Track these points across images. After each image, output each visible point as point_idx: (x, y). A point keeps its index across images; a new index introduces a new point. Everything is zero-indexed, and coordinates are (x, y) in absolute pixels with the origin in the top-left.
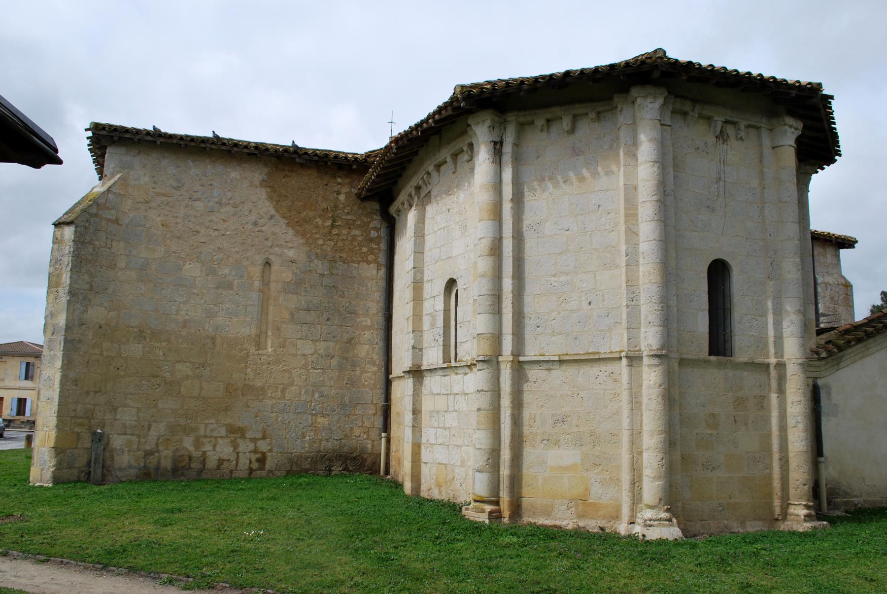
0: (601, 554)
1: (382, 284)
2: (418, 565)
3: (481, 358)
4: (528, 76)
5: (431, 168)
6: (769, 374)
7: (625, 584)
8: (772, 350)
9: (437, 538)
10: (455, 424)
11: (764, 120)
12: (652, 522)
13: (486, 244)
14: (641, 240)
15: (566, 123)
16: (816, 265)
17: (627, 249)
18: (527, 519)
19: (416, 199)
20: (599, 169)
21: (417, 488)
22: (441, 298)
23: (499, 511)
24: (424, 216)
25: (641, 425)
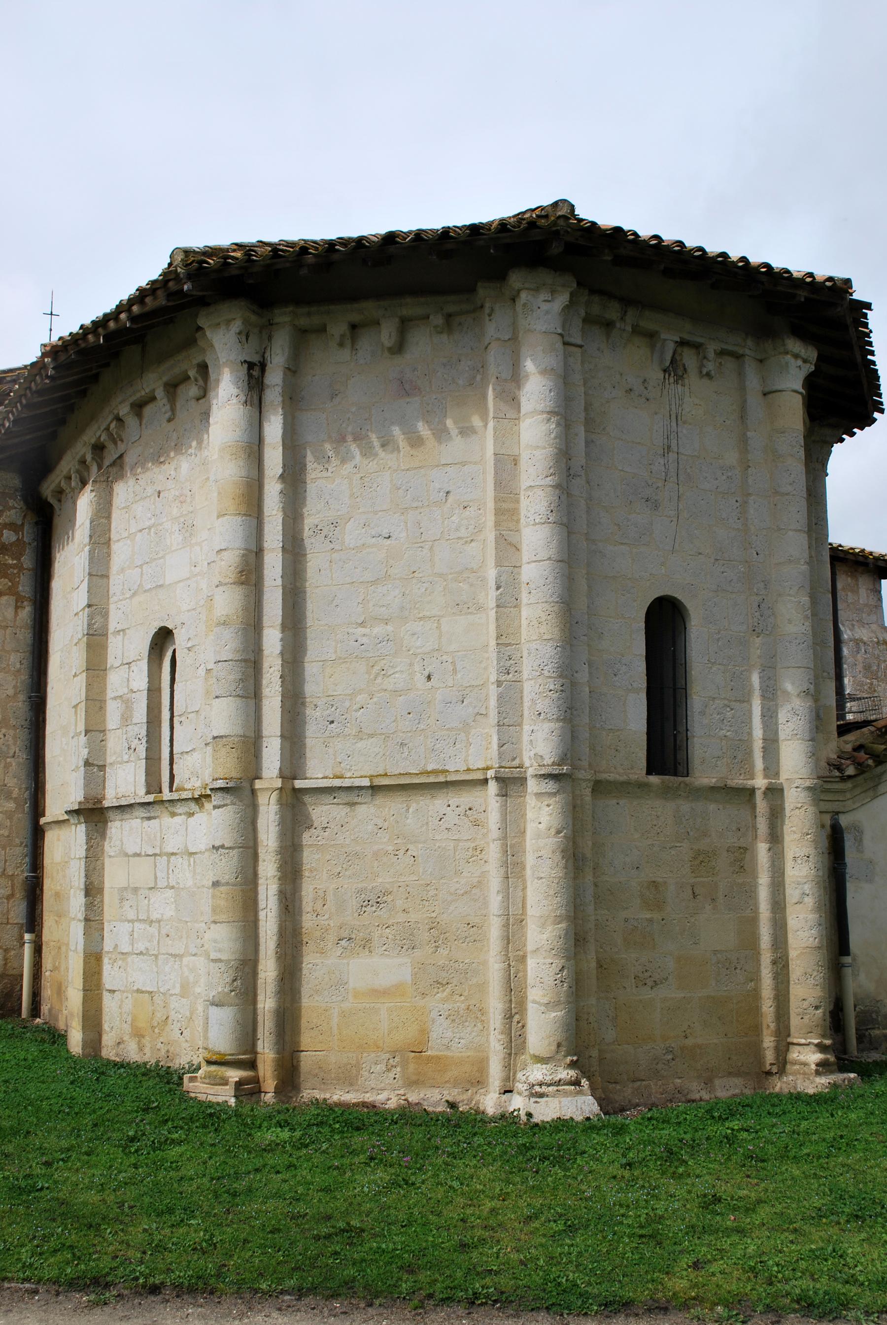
0: (450, 1154)
1: (26, 636)
2: (93, 1197)
3: (220, 784)
4: (317, 238)
5: (124, 410)
6: (754, 807)
7: (493, 1210)
8: (759, 764)
9: (132, 1140)
10: (169, 912)
11: (749, 342)
12: (544, 1089)
13: (230, 561)
14: (525, 559)
15: (387, 334)
16: (840, 606)
17: (499, 576)
18: (309, 1093)
19: (94, 468)
20: (449, 423)
21: (94, 1041)
22: (142, 668)
23: (256, 1080)
24: (109, 503)
25: (524, 907)
